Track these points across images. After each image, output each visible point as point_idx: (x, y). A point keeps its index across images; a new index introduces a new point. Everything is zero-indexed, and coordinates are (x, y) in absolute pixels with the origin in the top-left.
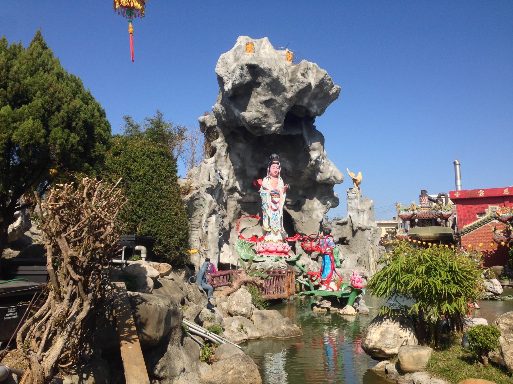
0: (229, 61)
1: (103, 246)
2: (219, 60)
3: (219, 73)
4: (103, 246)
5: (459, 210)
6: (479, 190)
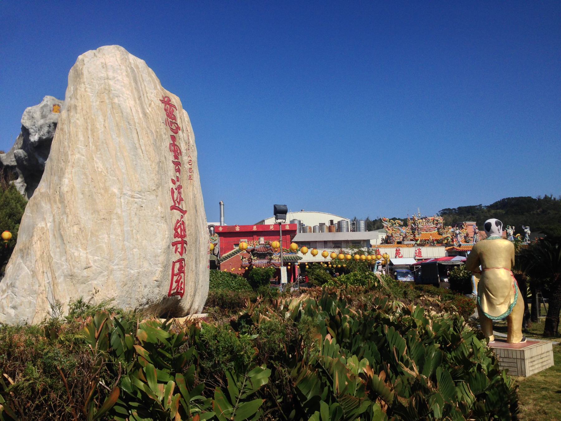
0: (35, 116)
1: (454, 313)
2: (25, 113)
3: (25, 125)
4: (454, 313)
5: (221, 242)
6: (236, 226)
